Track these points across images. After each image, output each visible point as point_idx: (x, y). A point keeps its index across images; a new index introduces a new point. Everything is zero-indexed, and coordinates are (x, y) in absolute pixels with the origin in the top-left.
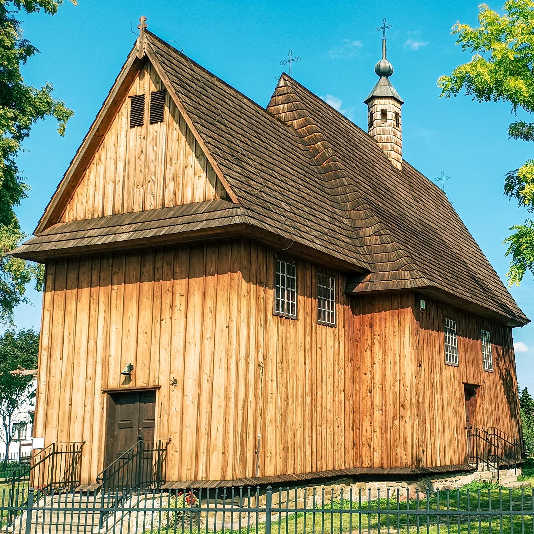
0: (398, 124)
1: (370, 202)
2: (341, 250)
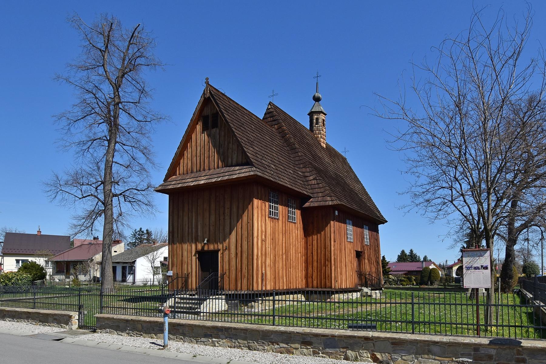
0: (324, 125)
1: (311, 163)
2: (298, 187)
